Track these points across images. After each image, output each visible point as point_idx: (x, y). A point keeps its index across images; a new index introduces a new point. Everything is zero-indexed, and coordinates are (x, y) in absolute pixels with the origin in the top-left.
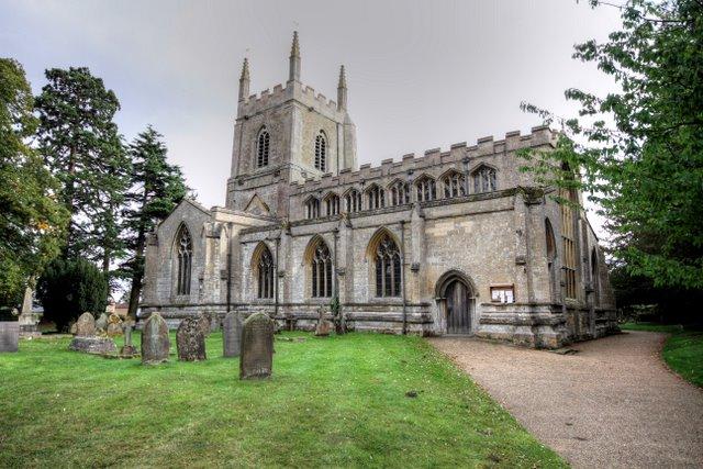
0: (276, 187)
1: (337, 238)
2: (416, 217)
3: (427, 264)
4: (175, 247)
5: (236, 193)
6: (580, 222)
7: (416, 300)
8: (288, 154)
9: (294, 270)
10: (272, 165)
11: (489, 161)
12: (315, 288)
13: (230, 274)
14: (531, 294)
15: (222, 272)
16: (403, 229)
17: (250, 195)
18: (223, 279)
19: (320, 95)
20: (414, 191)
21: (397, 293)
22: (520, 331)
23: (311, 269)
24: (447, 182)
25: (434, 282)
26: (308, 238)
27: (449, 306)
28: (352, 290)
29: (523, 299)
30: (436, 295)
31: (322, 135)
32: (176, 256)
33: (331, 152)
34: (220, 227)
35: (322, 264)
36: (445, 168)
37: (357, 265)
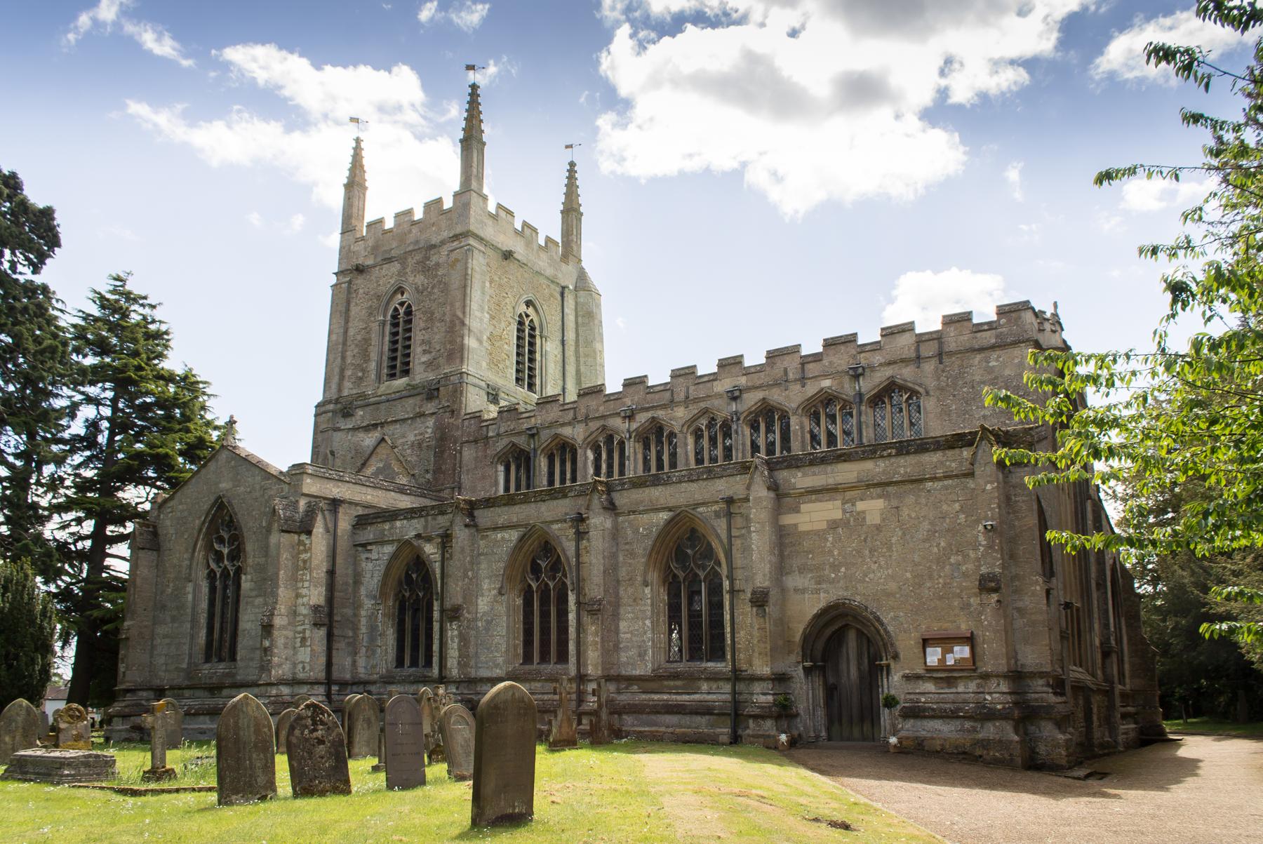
0: (431, 422)
1: (580, 535)
2: (760, 491)
3: (783, 590)
4: (200, 555)
5: (338, 436)
6: (1089, 504)
7: (762, 668)
8: (456, 352)
9: (483, 604)
10: (420, 374)
11: (906, 374)
12: (528, 643)
13: (330, 615)
14: (1012, 655)
15: (316, 609)
16: (729, 515)
17: (369, 440)
18: (316, 625)
19: (525, 224)
20: (744, 433)
21: (717, 653)
22: (990, 731)
23: (519, 602)
24: (816, 417)
25: (798, 637)
26: (514, 535)
27: (831, 680)
28: (617, 647)
29: (994, 661)
30: (804, 658)
31: (531, 311)
32: (202, 573)
33: (549, 349)
34: (311, 513)
35: (545, 592)
36: (811, 389)
37: (625, 593)
